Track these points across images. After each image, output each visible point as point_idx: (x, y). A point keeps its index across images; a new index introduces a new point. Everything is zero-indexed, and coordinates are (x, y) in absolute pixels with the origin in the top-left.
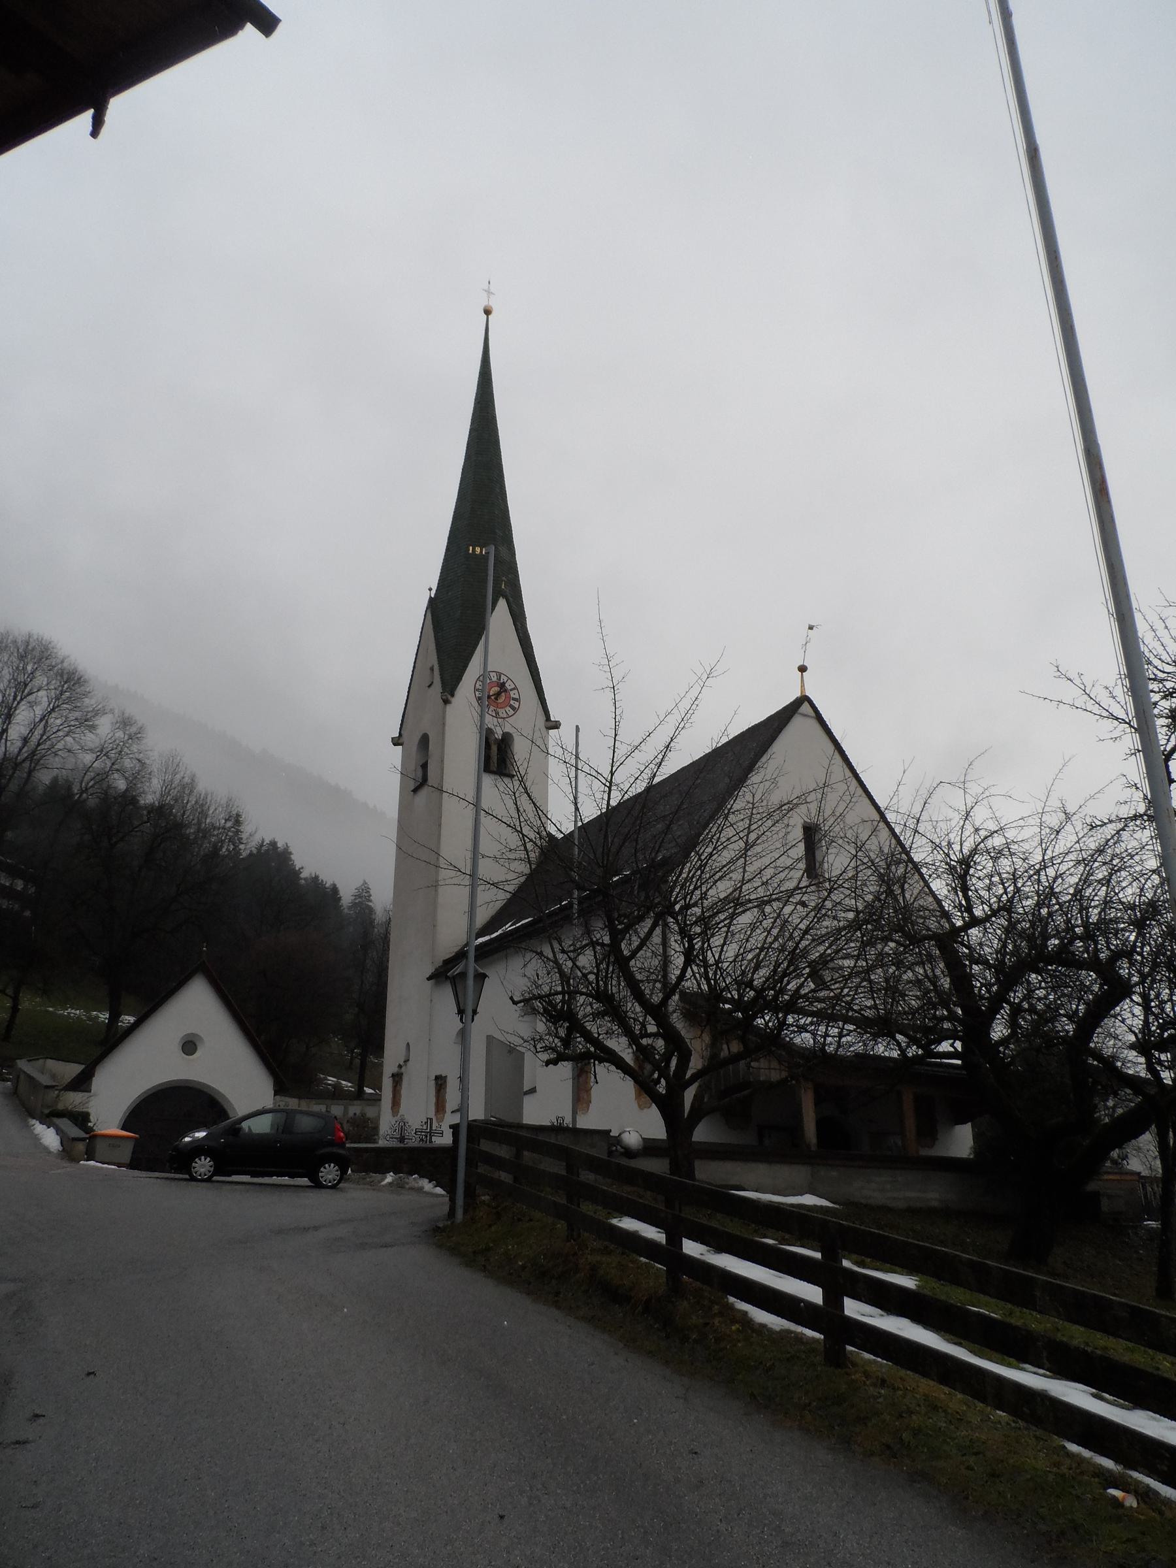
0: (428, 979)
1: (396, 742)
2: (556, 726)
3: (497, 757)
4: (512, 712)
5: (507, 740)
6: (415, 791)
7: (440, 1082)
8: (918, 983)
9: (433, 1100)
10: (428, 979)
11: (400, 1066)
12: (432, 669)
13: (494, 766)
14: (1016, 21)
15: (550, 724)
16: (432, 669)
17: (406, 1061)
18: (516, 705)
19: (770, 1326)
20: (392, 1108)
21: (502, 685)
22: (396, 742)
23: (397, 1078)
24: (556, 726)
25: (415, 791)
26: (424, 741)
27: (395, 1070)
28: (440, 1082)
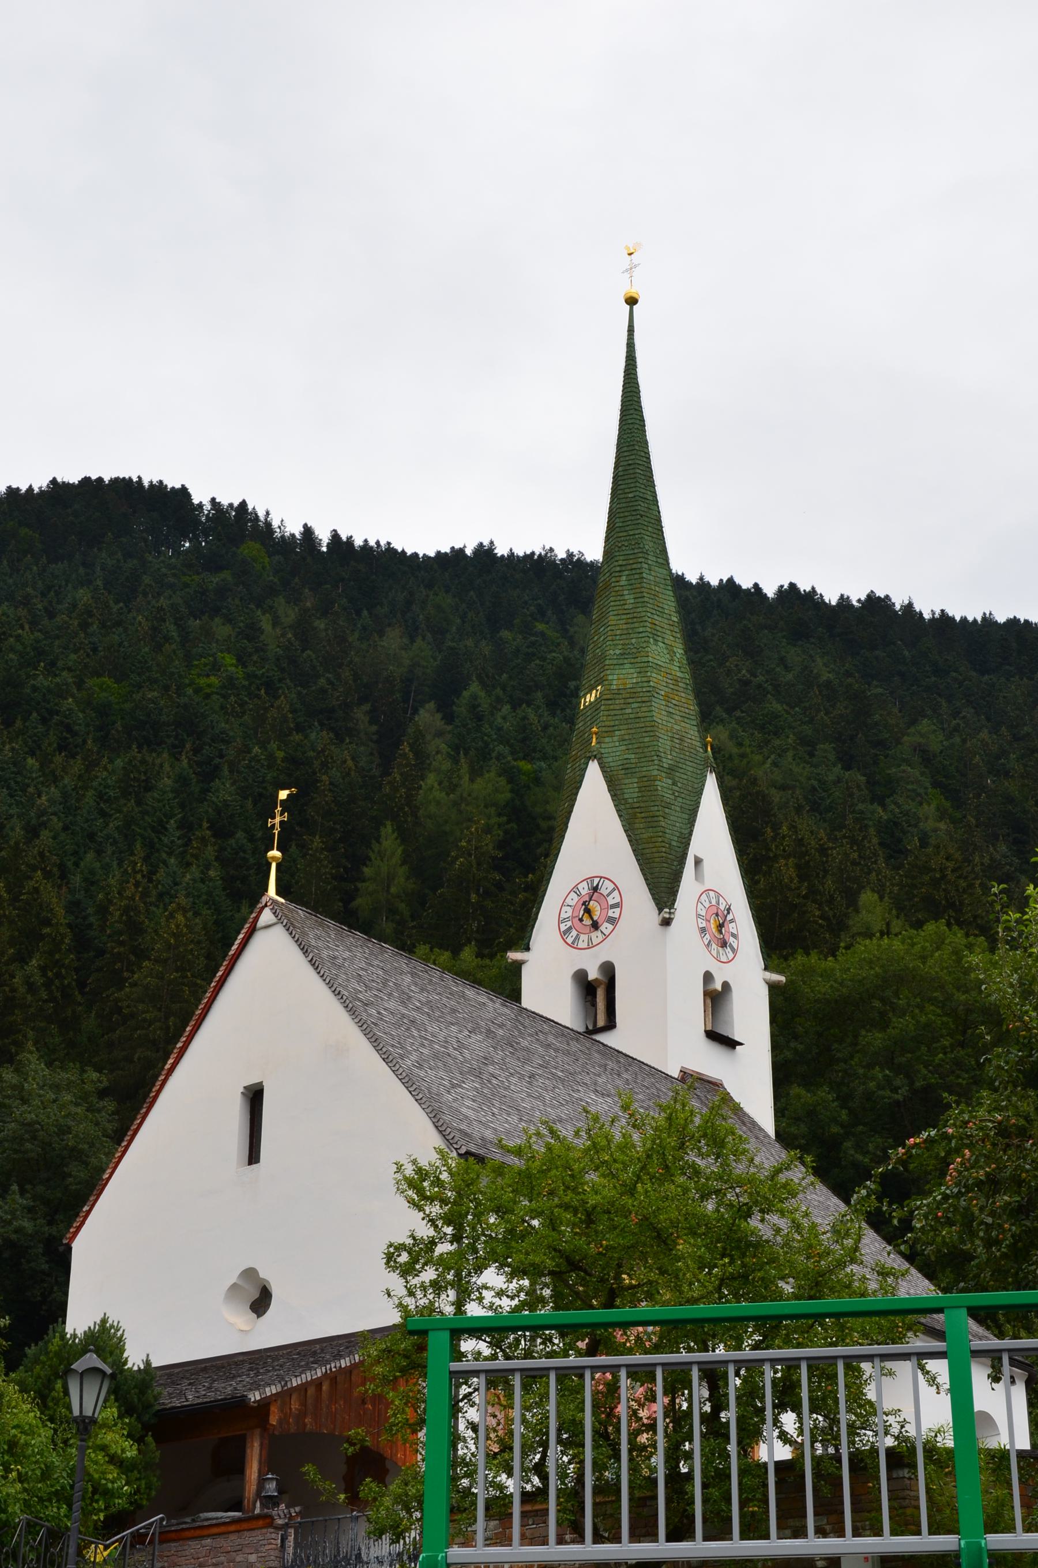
21: (724, 944)
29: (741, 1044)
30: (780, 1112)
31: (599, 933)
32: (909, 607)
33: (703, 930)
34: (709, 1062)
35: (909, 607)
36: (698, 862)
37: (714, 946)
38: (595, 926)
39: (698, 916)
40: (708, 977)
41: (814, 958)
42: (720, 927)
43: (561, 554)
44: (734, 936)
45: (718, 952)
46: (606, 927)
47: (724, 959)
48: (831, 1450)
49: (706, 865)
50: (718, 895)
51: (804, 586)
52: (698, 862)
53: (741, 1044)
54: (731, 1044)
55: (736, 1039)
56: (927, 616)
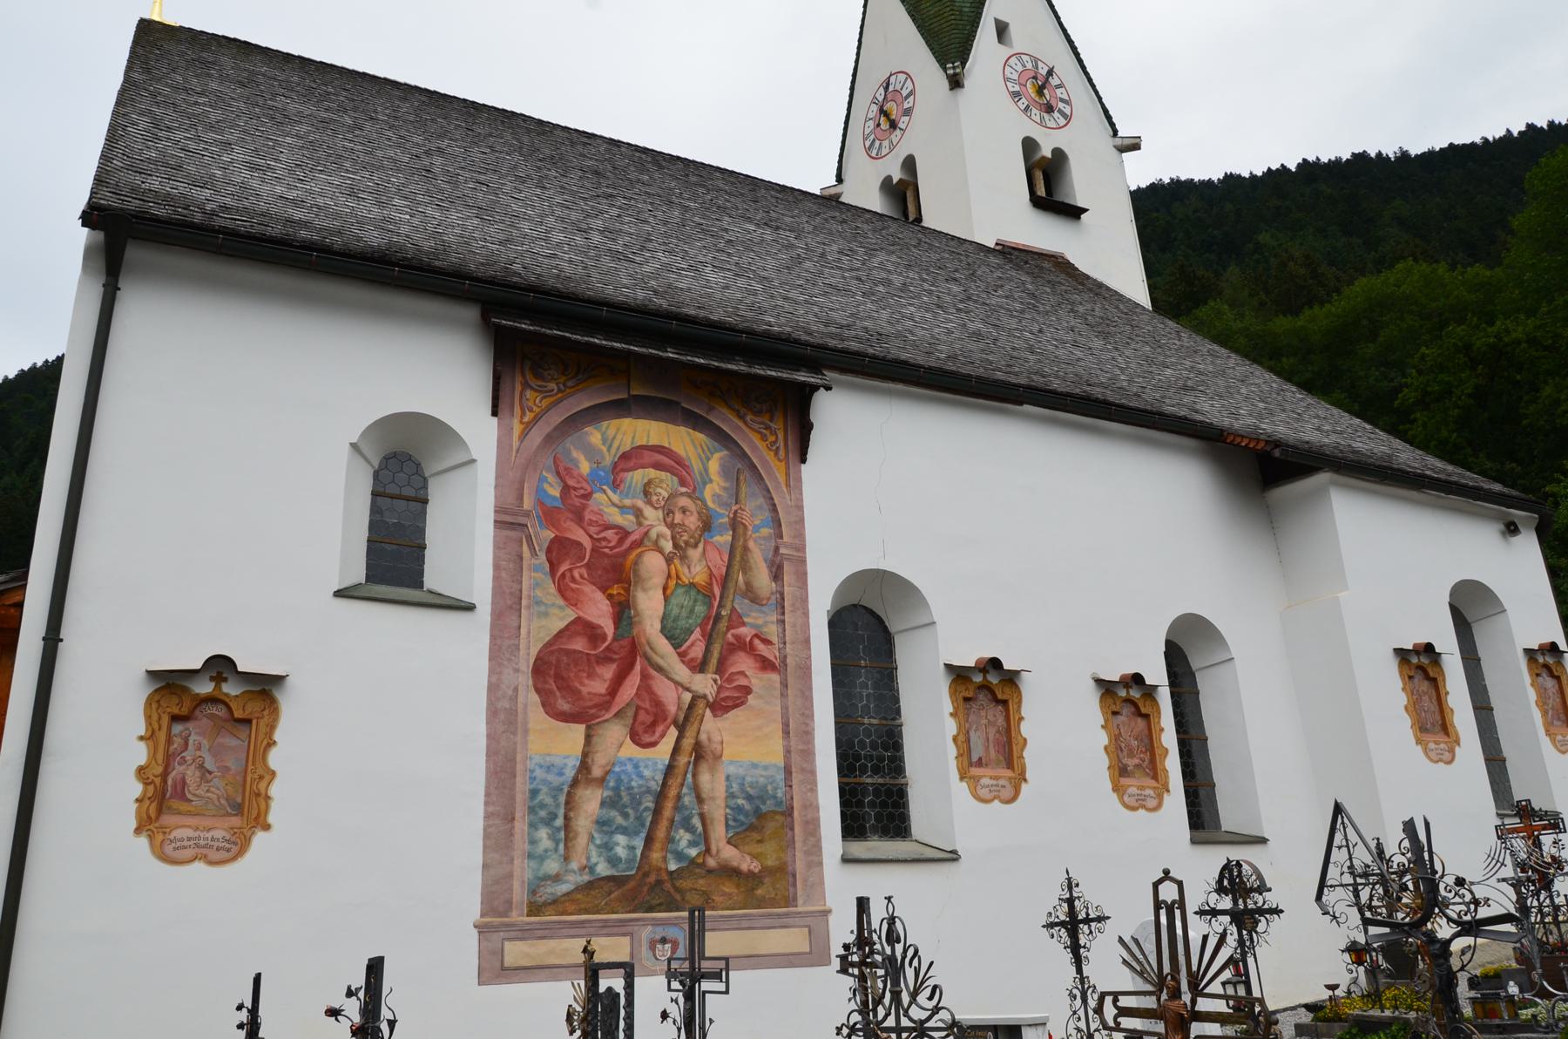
2: (1134, 146)
4: (1062, 121)
5: (1059, 156)
15: (1118, 142)
21: (1049, 109)
29: (1085, 210)
30: (1152, 289)
31: (898, 132)
32: (1379, 154)
33: (1016, 95)
34: (1043, 234)
35: (1379, 154)
36: (1002, 30)
37: (1034, 111)
38: (893, 125)
39: (1006, 79)
40: (1029, 145)
41: (1316, 309)
42: (1040, 91)
43: (1167, 181)
44: (1067, 102)
45: (1042, 118)
46: (903, 122)
47: (1052, 124)
48: (599, 610)
49: (1014, 31)
50: (1035, 60)
51: (1311, 158)
52: (1002, 30)
53: (1085, 210)
54: (1073, 213)
55: (1080, 204)
56: (1392, 156)
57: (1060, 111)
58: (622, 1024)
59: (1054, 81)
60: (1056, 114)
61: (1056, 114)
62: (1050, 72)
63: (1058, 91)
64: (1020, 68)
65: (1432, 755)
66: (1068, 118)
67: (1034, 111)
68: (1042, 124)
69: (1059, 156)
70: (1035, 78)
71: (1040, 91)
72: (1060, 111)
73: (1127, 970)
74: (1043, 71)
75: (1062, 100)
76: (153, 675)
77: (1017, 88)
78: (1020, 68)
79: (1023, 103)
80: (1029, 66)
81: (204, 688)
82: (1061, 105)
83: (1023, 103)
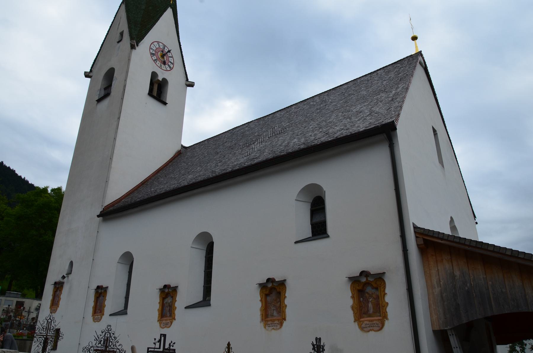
0: (98, 216)
1: (87, 75)
2: (192, 85)
3: (158, 90)
4: (169, 69)
5: (165, 82)
6: (99, 101)
7: (101, 292)
8: (376, 283)
9: (92, 304)
10: (98, 216)
11: (64, 277)
12: (122, 34)
13: (155, 94)
14: (398, 233)
15: (188, 83)
16: (122, 34)
17: (69, 273)
18: (172, 66)
19: (310, 207)
20: (51, 308)
21: (164, 63)
22: (87, 75)
23: (58, 286)
24: (192, 85)
25: (99, 101)
26: (110, 75)
27: (58, 279)
28: (101, 292)
33: (152, 54)
39: (150, 48)
40: (154, 75)
42: (163, 56)
44: (173, 64)
50: (165, 46)
57: (169, 65)
58: (440, 241)
59: (169, 55)
60: (167, 66)
61: (167, 66)
62: (169, 51)
63: (170, 59)
64: (157, 47)
65: (162, 326)
66: (171, 69)
67: (158, 62)
68: (160, 67)
69: (165, 82)
70: (162, 51)
71: (163, 56)
72: (169, 65)
73: (59, 343)
74: (166, 50)
75: (170, 62)
76: (350, 278)
77: (154, 52)
78: (157, 47)
79: (155, 58)
80: (162, 47)
81: (364, 280)
82: (169, 64)
83: (155, 58)
